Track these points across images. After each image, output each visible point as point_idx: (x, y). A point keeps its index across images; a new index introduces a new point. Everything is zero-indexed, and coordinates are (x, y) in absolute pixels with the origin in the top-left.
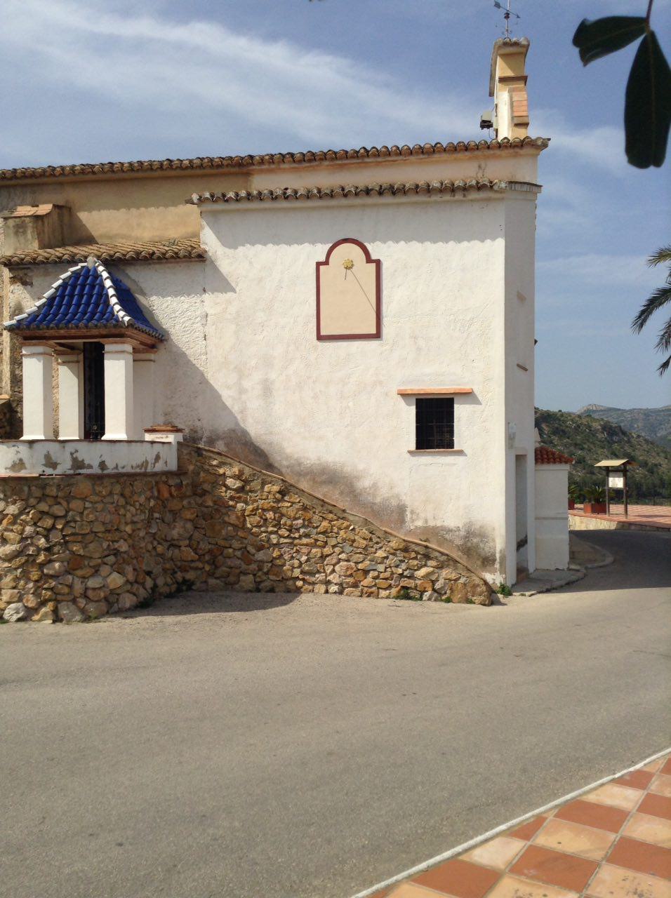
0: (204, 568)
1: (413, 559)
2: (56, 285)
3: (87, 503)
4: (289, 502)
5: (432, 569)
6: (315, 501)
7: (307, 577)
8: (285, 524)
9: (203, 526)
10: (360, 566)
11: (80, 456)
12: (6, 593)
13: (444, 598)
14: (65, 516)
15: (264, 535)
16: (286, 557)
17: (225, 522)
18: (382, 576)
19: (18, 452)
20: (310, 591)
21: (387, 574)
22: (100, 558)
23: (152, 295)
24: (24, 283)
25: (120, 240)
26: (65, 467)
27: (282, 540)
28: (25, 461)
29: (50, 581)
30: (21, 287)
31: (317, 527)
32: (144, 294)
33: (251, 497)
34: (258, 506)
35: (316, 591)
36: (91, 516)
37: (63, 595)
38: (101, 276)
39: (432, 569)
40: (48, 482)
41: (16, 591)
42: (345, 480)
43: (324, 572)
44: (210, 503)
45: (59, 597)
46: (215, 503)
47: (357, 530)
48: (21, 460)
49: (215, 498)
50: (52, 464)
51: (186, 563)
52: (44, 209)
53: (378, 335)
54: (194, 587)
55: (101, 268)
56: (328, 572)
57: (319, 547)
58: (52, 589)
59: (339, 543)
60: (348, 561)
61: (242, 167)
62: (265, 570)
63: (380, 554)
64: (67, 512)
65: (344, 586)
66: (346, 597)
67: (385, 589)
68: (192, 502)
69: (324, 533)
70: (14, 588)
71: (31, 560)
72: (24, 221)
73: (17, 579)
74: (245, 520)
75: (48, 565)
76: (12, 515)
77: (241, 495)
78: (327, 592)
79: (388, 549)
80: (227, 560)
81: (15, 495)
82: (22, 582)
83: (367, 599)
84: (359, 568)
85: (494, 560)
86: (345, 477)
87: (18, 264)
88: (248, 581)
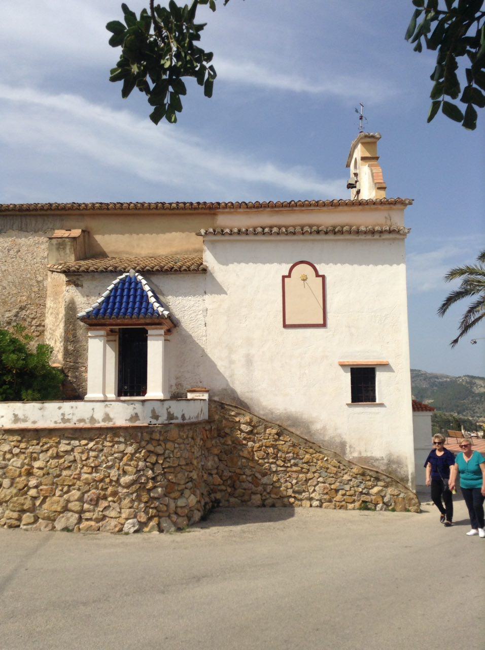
0: (226, 490)
1: (368, 481)
2: (110, 288)
3: (176, 445)
4: (283, 441)
5: (381, 488)
6: (301, 440)
7: (297, 495)
8: (281, 457)
9: (226, 459)
10: (333, 487)
11: (172, 410)
12: (125, 512)
13: (390, 508)
14: (163, 454)
15: (267, 465)
16: (282, 481)
17: (240, 456)
18: (348, 493)
19: (135, 408)
20: (300, 506)
21: (352, 492)
22: (184, 484)
23: (168, 296)
24: (77, 285)
25: (125, 255)
26: (163, 419)
27: (280, 469)
28: (139, 415)
29: (155, 502)
30: (74, 288)
31: (302, 459)
32: (163, 295)
33: (257, 438)
34: (262, 444)
35: (304, 505)
36: (179, 453)
37: (163, 512)
38: (141, 282)
39: (381, 488)
40: (153, 429)
41: (132, 510)
42: (304, 424)
43: (308, 491)
44: (230, 443)
45: (161, 514)
46: (233, 442)
47: (330, 461)
48: (136, 414)
49: (232, 439)
50: (156, 416)
51: (216, 487)
52: (76, 233)
53: (324, 325)
54: (221, 505)
55: (140, 277)
56: (311, 491)
57: (304, 473)
58: (155, 508)
59: (317, 470)
60: (324, 483)
61: (211, 210)
62: (268, 491)
63: (346, 477)
64: (165, 451)
65: (323, 501)
66: (325, 509)
67: (351, 503)
68: (218, 441)
69: (306, 463)
70: (130, 508)
71: (143, 487)
72: (65, 241)
73: (132, 501)
74: (254, 454)
75: (153, 490)
76: (130, 454)
77: (251, 436)
78: (311, 506)
79: (351, 474)
80: (243, 484)
81: (132, 439)
82: (136, 503)
83: (340, 510)
84: (332, 488)
85: (408, 480)
86: (303, 422)
87: (74, 271)
88: (257, 499)
